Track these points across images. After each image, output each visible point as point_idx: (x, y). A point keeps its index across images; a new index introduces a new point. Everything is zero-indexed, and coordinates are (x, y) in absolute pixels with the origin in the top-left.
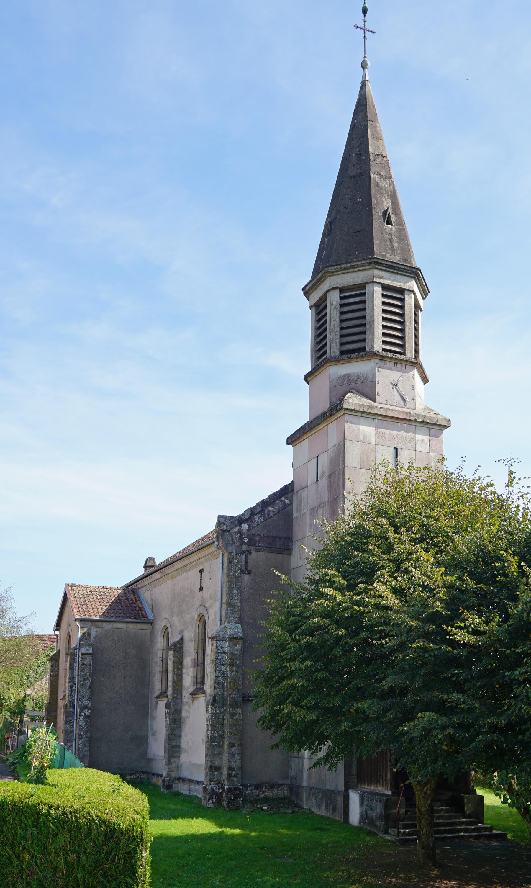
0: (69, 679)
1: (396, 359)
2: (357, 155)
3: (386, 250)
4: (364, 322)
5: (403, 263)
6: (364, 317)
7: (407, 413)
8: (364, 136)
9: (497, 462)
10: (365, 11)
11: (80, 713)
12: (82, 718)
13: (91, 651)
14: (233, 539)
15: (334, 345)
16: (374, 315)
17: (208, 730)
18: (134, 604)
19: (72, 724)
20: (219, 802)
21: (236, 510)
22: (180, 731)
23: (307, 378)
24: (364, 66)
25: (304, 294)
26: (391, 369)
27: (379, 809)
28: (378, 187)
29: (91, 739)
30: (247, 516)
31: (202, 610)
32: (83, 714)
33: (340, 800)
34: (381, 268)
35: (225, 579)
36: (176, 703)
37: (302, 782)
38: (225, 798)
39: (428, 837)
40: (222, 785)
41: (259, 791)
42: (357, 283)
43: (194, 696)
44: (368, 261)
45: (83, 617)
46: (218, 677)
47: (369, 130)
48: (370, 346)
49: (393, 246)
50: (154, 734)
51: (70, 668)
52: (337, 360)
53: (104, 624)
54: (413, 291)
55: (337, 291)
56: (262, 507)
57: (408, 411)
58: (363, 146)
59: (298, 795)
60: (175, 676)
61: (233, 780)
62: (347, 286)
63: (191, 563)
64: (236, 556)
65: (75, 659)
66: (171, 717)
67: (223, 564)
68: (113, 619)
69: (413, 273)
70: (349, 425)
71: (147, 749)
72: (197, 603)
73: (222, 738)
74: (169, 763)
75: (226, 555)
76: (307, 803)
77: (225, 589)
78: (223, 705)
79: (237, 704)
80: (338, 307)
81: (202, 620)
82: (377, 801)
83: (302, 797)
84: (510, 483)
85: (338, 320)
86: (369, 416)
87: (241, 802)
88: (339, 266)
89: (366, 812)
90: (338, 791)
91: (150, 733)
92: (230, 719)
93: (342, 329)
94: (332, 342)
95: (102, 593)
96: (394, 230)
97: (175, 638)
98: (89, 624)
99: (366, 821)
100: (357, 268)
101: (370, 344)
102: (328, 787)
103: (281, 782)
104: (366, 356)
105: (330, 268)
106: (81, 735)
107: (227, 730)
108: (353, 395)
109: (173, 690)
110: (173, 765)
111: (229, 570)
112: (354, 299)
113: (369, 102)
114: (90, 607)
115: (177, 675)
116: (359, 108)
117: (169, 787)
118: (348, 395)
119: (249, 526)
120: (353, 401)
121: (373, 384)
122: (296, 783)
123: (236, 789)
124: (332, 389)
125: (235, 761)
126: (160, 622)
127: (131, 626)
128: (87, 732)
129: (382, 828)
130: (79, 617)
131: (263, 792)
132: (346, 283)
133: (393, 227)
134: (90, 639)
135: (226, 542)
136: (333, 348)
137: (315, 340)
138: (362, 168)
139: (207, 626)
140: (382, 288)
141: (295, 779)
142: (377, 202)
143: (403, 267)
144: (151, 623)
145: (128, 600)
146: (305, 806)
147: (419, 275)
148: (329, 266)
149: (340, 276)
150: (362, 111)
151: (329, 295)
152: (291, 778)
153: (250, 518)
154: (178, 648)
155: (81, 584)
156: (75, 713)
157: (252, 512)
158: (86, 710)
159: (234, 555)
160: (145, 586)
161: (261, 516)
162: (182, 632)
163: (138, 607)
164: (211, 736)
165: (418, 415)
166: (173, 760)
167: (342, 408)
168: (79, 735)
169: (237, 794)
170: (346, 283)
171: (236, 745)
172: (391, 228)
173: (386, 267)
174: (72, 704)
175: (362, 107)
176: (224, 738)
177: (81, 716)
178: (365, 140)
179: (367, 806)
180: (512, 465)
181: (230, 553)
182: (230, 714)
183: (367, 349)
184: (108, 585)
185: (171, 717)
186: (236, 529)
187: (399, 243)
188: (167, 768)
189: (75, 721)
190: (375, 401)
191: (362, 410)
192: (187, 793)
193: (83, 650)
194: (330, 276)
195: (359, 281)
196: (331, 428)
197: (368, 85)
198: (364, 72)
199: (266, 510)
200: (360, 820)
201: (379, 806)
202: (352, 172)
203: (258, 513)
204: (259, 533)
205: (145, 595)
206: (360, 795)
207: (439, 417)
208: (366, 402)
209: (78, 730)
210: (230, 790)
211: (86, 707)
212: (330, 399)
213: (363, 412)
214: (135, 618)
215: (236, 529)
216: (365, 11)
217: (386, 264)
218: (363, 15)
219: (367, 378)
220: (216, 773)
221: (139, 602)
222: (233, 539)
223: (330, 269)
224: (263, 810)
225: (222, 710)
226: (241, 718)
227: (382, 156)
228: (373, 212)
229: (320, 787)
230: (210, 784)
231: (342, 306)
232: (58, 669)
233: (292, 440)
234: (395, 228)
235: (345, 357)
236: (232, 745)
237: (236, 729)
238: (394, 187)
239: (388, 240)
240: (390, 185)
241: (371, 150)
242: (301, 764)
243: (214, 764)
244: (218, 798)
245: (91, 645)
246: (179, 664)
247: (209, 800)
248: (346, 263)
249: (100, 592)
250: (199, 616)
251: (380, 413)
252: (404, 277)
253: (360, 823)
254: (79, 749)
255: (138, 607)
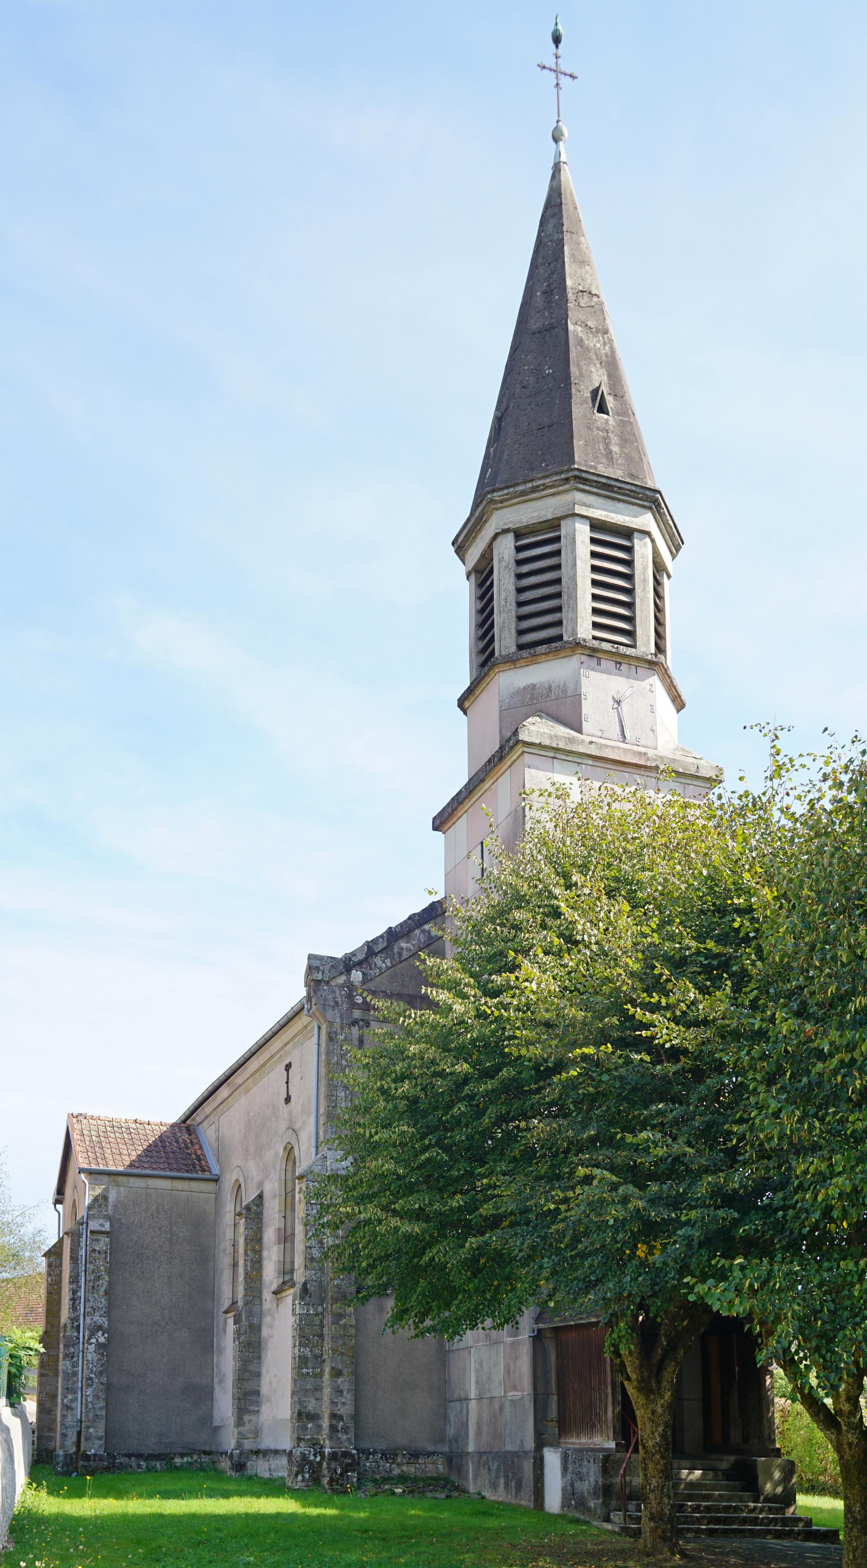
0: (70, 1277)
1: (618, 654)
2: (544, 293)
3: (596, 457)
4: (558, 590)
5: (628, 480)
6: (558, 581)
7: (640, 753)
8: (556, 260)
9: (748, 728)
10: (557, 39)
11: (89, 1339)
12: (92, 1348)
13: (107, 1227)
14: (335, 998)
15: (506, 634)
16: (575, 575)
17: (294, 1346)
18: (188, 1148)
19: (75, 1359)
20: (316, 1479)
21: (342, 944)
22: (260, 1364)
23: (463, 703)
24: (556, 138)
25: (456, 552)
26: (610, 673)
27: (593, 1475)
28: (581, 346)
29: (108, 1388)
30: (361, 957)
31: (289, 1137)
32: (93, 1341)
33: (528, 1467)
34: (587, 488)
35: (323, 1070)
36: (250, 1314)
37: (467, 1445)
38: (326, 1472)
39: (661, 1498)
40: (321, 1448)
41: (391, 1463)
42: (544, 519)
43: (279, 1296)
44: (563, 476)
45: (94, 1167)
46: (310, 1248)
47: (566, 248)
48: (569, 633)
49: (611, 452)
50: (221, 1381)
51: (71, 1258)
52: (511, 661)
53: (132, 1180)
54: (648, 534)
55: (511, 536)
56: (388, 940)
57: (643, 750)
58: (555, 276)
59: (460, 1471)
60: (249, 1264)
61: (339, 1439)
62: (527, 526)
63: (273, 1056)
64: (342, 1028)
65: (79, 1242)
66: (242, 1338)
67: (319, 1045)
68: (148, 1172)
69: (647, 499)
70: (533, 771)
71: (212, 1409)
72: (283, 1125)
73: (319, 1360)
74: (240, 1423)
75: (324, 1027)
76: (475, 1482)
77: (323, 1090)
78: (322, 1301)
79: (345, 1297)
80: (512, 564)
81: (291, 1157)
82: (589, 1461)
83: (467, 1472)
84: (778, 771)
85: (512, 589)
86: (570, 758)
87: (355, 1480)
88: (511, 490)
89: (572, 1485)
90: (525, 1452)
91: (216, 1380)
92: (333, 1324)
93: (520, 604)
94: (502, 629)
95: (132, 1130)
96: (611, 422)
97: (250, 1196)
98: (106, 1178)
99: (573, 1502)
100: (543, 490)
101: (570, 628)
102: (509, 1447)
103: (431, 1448)
104: (562, 648)
105: (495, 494)
106: (91, 1379)
107: (328, 1345)
108: (539, 720)
109: (246, 1290)
110: (247, 1427)
111: (329, 1053)
112: (541, 547)
113: (566, 199)
114: (109, 1151)
115: (252, 1261)
116: (549, 211)
117: (240, 1467)
118: (530, 720)
119: (364, 974)
120: (537, 729)
121: (577, 699)
122: (458, 1447)
123: (346, 1454)
124: (504, 712)
125: (344, 1404)
126: (229, 1176)
127: (179, 1185)
128: (101, 1373)
129: (599, 1511)
130: (86, 1166)
131: (399, 1465)
132: (524, 520)
133: (610, 418)
134: (106, 1206)
135: (322, 1002)
136: (505, 640)
137: (476, 632)
138: (554, 316)
139: (297, 1164)
140: (591, 526)
141: (457, 1441)
142: (581, 374)
143: (629, 487)
144: (216, 1181)
145: (177, 1142)
146: (472, 1489)
147: (659, 504)
148: (493, 491)
149: (514, 508)
150: (554, 215)
151: (495, 545)
152: (450, 1441)
153: (366, 958)
154: (253, 1213)
155: (96, 1114)
156: (81, 1340)
157: (371, 949)
158: (100, 1333)
159: (337, 1026)
160: (207, 1117)
161: (386, 958)
162: (261, 1184)
163: (195, 1154)
164: (299, 1357)
165: (661, 757)
166: (246, 1418)
167: (518, 742)
168: (88, 1379)
169: (348, 1465)
170: (524, 520)
171: (345, 1372)
172: (607, 420)
173: (595, 487)
174: (76, 1324)
175: (554, 208)
176: (324, 1361)
177: (91, 1344)
178: (558, 266)
179: (573, 1473)
180: (777, 737)
181: (331, 1024)
182: (334, 1315)
183: (565, 638)
184: (143, 1118)
185: (242, 1338)
186: (341, 980)
187: (622, 447)
188: (236, 1433)
189: (81, 1354)
190: (579, 730)
191: (554, 745)
192: (267, 1475)
193: (94, 1225)
194: (497, 509)
195: (550, 522)
196: (502, 786)
197: (565, 171)
198: (558, 146)
199: (396, 947)
200: (562, 1503)
201: (592, 1470)
202: (535, 324)
203: (381, 951)
204: (383, 989)
205: (208, 1134)
206: (562, 1454)
207: (702, 763)
208: (563, 731)
209: (85, 1371)
210: (334, 1456)
211: (100, 1328)
212: (501, 732)
213: (557, 750)
214: (187, 1171)
215: (341, 980)
216: (557, 39)
217: (596, 482)
218: (554, 46)
219: (564, 691)
220: (310, 1425)
221: (197, 1147)
222: (335, 998)
223: (496, 496)
224: (394, 1493)
225: (320, 1309)
226: (354, 1322)
227: (590, 293)
228: (573, 391)
229: (496, 1450)
230: (298, 1446)
231: (519, 563)
232: (61, 1272)
233: (441, 822)
234: (615, 420)
235: (524, 653)
236: (337, 1373)
237: (344, 1344)
238: (612, 348)
239: (600, 440)
240: (605, 344)
241: (569, 282)
242: (465, 1411)
243: (305, 1407)
244: (314, 1472)
245: (108, 1218)
246: (255, 1241)
247: (296, 1475)
248: (525, 483)
249: (128, 1128)
250: (285, 1148)
251: (589, 752)
252: (631, 507)
253: (563, 1507)
254: (87, 1405)
255: (195, 1154)
